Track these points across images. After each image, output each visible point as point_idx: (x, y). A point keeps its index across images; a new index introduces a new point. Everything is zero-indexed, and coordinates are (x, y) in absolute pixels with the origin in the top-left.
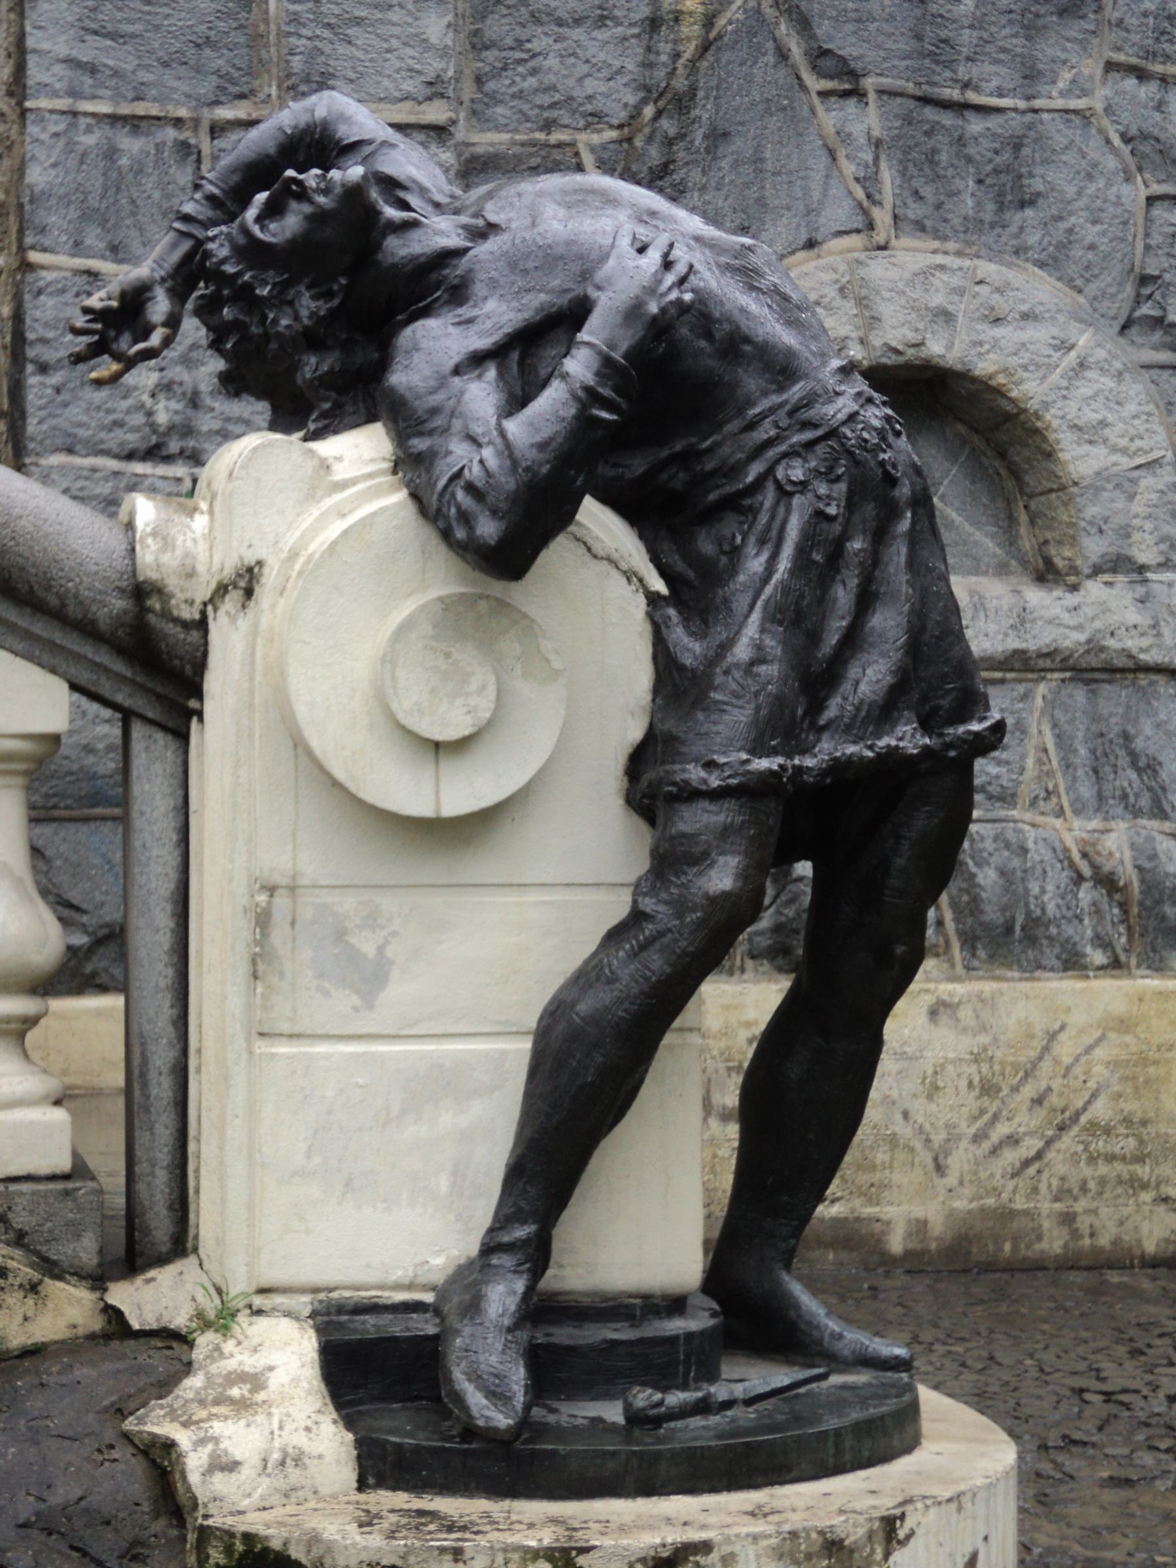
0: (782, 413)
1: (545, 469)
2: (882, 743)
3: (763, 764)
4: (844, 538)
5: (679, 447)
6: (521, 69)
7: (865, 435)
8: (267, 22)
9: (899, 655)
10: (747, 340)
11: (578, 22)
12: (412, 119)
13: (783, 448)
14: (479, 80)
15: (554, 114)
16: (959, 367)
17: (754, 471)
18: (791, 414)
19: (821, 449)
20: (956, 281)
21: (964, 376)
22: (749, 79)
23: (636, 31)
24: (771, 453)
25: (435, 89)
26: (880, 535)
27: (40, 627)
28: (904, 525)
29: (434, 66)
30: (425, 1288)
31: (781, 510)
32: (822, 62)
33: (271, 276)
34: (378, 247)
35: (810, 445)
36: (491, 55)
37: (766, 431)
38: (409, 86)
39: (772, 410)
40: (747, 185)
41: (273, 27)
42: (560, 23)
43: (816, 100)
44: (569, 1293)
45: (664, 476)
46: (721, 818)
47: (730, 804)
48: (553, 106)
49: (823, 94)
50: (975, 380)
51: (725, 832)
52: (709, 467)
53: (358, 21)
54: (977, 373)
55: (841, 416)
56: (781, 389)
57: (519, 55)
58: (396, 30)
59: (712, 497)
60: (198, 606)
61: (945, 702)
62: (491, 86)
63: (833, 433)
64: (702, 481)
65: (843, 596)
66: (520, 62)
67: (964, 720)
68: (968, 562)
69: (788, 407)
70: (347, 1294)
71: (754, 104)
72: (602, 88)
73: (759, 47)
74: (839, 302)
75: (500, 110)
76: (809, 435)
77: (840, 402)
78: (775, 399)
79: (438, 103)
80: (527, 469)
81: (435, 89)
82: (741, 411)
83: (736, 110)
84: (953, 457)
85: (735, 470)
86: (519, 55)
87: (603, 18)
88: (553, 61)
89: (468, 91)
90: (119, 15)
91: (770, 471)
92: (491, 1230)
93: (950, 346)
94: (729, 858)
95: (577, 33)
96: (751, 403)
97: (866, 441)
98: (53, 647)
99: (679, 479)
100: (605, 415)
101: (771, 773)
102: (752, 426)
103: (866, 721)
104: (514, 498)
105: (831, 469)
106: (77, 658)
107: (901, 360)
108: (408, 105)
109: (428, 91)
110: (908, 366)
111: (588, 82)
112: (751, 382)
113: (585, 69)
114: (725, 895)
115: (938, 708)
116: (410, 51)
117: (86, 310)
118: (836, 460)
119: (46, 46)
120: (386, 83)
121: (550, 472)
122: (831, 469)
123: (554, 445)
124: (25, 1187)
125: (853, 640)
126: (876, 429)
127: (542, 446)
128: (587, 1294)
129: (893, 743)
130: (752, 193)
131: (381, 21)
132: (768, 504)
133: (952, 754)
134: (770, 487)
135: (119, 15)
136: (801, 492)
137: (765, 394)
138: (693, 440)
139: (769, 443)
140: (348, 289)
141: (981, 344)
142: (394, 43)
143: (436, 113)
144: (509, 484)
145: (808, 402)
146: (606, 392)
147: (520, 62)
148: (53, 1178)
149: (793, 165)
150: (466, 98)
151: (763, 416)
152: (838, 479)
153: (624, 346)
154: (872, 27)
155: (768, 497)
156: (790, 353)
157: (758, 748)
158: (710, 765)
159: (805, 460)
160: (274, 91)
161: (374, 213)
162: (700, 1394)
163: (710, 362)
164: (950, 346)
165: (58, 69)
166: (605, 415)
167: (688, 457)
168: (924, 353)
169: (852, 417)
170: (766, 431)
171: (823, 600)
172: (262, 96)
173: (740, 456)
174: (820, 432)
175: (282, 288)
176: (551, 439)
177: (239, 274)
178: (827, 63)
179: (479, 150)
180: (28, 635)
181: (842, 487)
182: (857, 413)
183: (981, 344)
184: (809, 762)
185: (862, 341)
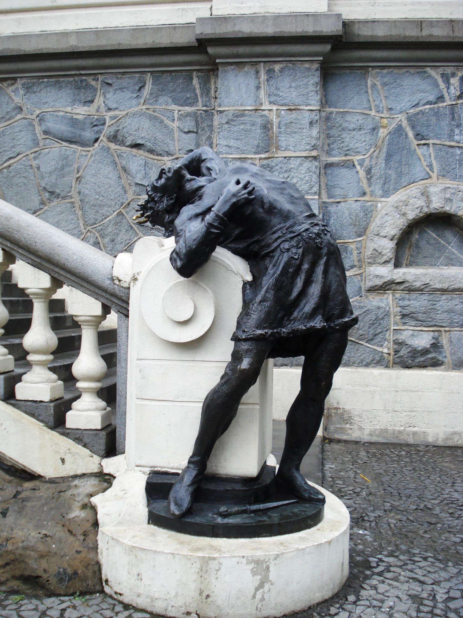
0: (285, 229)
1: (194, 247)
2: (308, 325)
3: (259, 332)
4: (301, 264)
5: (256, 238)
6: (340, 142)
7: (310, 235)
8: (273, 134)
9: (317, 299)
10: (275, 208)
11: (354, 130)
12: (308, 155)
13: (283, 239)
14: (329, 145)
15: (347, 152)
16: (453, 213)
17: (275, 245)
18: (287, 229)
19: (296, 239)
20: (453, 191)
21: (455, 216)
22: (398, 142)
23: (369, 131)
24: (279, 241)
25: (314, 147)
26: (314, 265)
27: (92, 288)
28: (323, 261)
29: (314, 142)
30: (179, 469)
31: (281, 257)
32: (417, 137)
33: (159, 195)
34: (184, 186)
35: (292, 238)
36: (332, 139)
37: (279, 234)
38: (307, 147)
39: (281, 228)
40: (397, 168)
41: (275, 135)
42: (350, 130)
43: (416, 147)
44: (220, 474)
45: (252, 247)
46: (246, 347)
47: (250, 343)
48: (348, 150)
49: (418, 145)
50: (458, 216)
51: (247, 351)
52: (264, 244)
53: (295, 132)
54: (459, 214)
55: (303, 230)
56: (285, 222)
57: (339, 139)
58: (305, 134)
59: (263, 253)
60: (128, 283)
61: (336, 312)
62: (332, 146)
63: (299, 235)
64: (262, 248)
65: (299, 283)
66: (339, 140)
67: (343, 318)
68: (459, 264)
69: (286, 227)
70: (159, 469)
71: (399, 148)
72: (360, 145)
73: (401, 134)
74: (421, 197)
75: (334, 152)
76: (292, 235)
77: (304, 225)
78: (282, 225)
79: (315, 151)
80: (189, 247)
81: (314, 147)
82: (272, 228)
83: (395, 150)
84: (455, 236)
85: (269, 245)
86: (339, 139)
87: (360, 129)
88: (347, 139)
89: (326, 148)
90: (239, 134)
91: (279, 245)
92: (191, 457)
93: (451, 208)
94: (247, 359)
95: (354, 132)
96: (274, 226)
97: (311, 237)
98: (94, 292)
99: (256, 248)
100: (216, 231)
101: (261, 334)
102: (274, 233)
103: (305, 318)
104: (186, 255)
105: (298, 245)
106: (102, 296)
107: (438, 211)
108: (307, 151)
109: (312, 148)
110: (440, 213)
111: (356, 144)
112: (275, 220)
113: (356, 141)
114: (244, 370)
115: (334, 314)
116: (308, 139)
117: (138, 205)
118: (299, 242)
119: (221, 143)
120: (302, 147)
121: (196, 247)
122: (298, 245)
123: (198, 239)
124: (87, 432)
125: (303, 293)
126: (315, 233)
127: (194, 240)
128: (224, 475)
129: (313, 325)
130: (399, 170)
131: (301, 132)
132: (277, 255)
133: (337, 328)
134: (279, 249)
135: (239, 134)
136: (287, 252)
137: (280, 223)
138: (259, 237)
139: (279, 238)
140: (176, 198)
141: (460, 207)
142: (304, 137)
143: (314, 153)
144: (184, 251)
145: (292, 226)
146: (216, 224)
147: (339, 140)
148: (96, 430)
149: (410, 162)
150: (325, 149)
151: (278, 230)
152: (300, 247)
153: (222, 212)
154: (431, 128)
155: (277, 254)
156: (289, 211)
157: (258, 327)
158: (244, 331)
159: (290, 242)
160: (275, 150)
161: (183, 176)
162: (244, 508)
163: (263, 215)
164: (451, 208)
165: (224, 148)
166: (216, 231)
167: (257, 242)
168: (444, 209)
169: (307, 230)
170: (279, 234)
171: (292, 284)
172: (271, 152)
173: (271, 241)
174: (296, 234)
175: (162, 197)
176: (197, 238)
177: (152, 195)
178: (419, 137)
179: (329, 162)
180: (90, 290)
181: (300, 251)
182: (309, 229)
183: (460, 207)
184: (284, 330)
185: (427, 207)
